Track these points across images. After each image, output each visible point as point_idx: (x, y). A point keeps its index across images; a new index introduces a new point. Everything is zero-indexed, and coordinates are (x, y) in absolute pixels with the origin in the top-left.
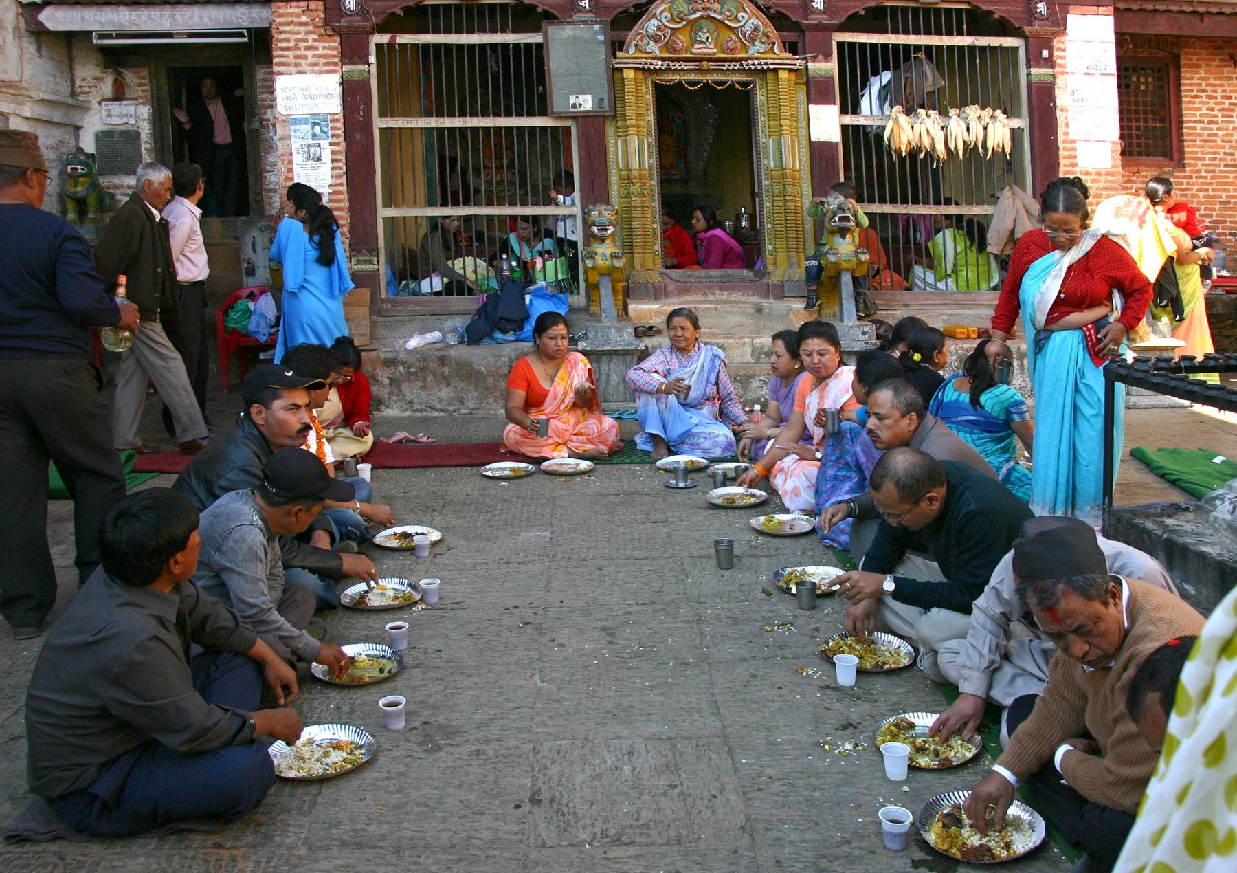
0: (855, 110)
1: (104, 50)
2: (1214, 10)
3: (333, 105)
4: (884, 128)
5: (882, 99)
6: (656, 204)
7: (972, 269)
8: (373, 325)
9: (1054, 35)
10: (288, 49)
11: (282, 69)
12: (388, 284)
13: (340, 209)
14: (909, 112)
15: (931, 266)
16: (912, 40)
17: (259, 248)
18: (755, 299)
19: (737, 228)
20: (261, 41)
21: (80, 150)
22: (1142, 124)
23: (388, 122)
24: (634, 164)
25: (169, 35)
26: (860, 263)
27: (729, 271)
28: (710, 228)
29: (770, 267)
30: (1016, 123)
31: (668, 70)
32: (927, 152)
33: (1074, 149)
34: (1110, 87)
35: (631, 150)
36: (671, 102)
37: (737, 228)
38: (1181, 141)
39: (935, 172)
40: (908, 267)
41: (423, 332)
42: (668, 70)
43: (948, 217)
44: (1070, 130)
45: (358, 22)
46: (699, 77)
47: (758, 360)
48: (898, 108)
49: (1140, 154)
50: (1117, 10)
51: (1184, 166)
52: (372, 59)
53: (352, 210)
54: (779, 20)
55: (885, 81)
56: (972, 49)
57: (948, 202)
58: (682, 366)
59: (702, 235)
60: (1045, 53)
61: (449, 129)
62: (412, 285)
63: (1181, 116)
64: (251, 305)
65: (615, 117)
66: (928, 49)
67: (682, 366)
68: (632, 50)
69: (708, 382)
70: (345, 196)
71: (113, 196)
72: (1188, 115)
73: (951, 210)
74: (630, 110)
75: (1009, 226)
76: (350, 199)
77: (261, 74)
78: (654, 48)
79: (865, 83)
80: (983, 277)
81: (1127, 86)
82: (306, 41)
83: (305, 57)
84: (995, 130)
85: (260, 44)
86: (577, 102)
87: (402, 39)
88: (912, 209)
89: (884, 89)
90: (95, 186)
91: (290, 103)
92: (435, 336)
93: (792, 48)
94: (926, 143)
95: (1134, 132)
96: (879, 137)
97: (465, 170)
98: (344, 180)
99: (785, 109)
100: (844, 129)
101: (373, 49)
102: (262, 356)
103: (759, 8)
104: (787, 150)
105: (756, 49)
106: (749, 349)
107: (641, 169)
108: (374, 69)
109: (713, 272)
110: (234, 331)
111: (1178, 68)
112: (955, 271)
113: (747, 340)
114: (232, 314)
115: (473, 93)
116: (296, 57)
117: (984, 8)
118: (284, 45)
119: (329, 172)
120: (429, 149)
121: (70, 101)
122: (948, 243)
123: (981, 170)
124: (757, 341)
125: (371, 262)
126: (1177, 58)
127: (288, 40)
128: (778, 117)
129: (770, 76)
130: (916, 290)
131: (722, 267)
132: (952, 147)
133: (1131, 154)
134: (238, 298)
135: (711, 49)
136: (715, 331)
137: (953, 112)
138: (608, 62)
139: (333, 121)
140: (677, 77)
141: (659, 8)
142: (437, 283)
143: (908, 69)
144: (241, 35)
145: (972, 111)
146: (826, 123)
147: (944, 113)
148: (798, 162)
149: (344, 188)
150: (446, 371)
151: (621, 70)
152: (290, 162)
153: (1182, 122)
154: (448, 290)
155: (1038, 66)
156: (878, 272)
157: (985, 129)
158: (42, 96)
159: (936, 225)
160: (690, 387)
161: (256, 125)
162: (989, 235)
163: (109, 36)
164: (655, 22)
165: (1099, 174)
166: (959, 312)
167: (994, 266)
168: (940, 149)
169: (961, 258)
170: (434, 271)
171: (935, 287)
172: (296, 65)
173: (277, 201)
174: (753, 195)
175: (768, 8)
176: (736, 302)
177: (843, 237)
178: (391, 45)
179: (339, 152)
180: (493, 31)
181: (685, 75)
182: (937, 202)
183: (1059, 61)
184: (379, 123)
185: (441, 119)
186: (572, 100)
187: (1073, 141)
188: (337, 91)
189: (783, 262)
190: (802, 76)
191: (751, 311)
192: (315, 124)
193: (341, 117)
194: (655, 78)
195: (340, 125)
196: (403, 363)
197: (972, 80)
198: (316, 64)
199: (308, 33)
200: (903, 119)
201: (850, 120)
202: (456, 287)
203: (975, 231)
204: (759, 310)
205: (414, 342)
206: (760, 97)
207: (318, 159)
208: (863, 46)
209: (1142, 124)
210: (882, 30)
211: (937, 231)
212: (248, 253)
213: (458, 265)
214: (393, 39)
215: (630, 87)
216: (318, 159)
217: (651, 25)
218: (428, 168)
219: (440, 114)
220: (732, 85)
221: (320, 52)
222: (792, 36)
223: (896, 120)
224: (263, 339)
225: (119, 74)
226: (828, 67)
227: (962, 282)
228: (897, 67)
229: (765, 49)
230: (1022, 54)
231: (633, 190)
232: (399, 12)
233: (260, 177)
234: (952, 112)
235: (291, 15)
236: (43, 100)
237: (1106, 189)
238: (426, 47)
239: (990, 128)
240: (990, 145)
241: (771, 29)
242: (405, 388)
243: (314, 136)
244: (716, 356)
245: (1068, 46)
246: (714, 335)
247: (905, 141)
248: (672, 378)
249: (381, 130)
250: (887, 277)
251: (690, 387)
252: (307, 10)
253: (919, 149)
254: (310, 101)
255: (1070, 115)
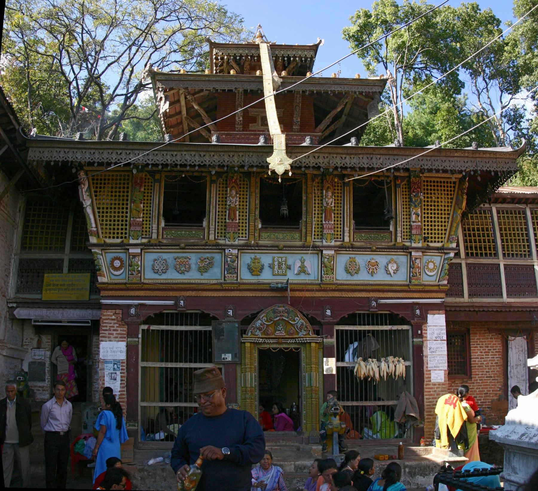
0: (343, 360)
1: (35, 326)
2: (481, 310)
3: (123, 356)
4: (354, 367)
5: (354, 354)
6: (257, 403)
7: (388, 428)
8: (135, 453)
9: (423, 323)
10: (106, 330)
11: (103, 339)
12: (142, 435)
13: (123, 402)
14: (364, 360)
15: (371, 428)
16: (367, 328)
17: (89, 418)
18: (297, 444)
19: (291, 412)
20: (96, 325)
21: (23, 370)
22: (456, 360)
23: (145, 364)
24: (248, 385)
25: (60, 322)
26: (342, 428)
27: (287, 432)
28: (280, 412)
29: (304, 430)
30: (408, 363)
31: (264, 343)
32: (372, 378)
33: (430, 374)
34: (444, 346)
35: (247, 378)
36: (265, 357)
37: (291, 412)
38: (470, 367)
39: (375, 386)
40: (362, 429)
41: (155, 457)
42: (264, 343)
43: (379, 406)
44: (429, 366)
45: (135, 319)
46: (278, 346)
47: (297, 471)
48: (360, 358)
49: (455, 374)
50: (446, 311)
51: (471, 378)
52: (140, 336)
53: (128, 403)
54: (312, 321)
55: (355, 346)
56: (391, 331)
57: (379, 399)
58: (264, 475)
59: (277, 416)
60: (419, 332)
61: (171, 368)
62: (152, 436)
63: (470, 356)
64: (85, 442)
65: (241, 364)
66: (373, 331)
67: (264, 475)
68: (250, 334)
69: (275, 482)
70: (125, 396)
71: (33, 390)
72: (473, 355)
73: (380, 403)
74: (247, 361)
75: (403, 409)
76: (127, 398)
77: (94, 340)
78: (259, 333)
79: (347, 347)
80: (392, 432)
81: (451, 344)
82: (113, 327)
83: (113, 334)
84: (399, 367)
85: (95, 326)
86: (225, 357)
87: (153, 327)
88: (365, 403)
89: (355, 350)
90: (27, 386)
91: (105, 354)
92: (160, 459)
93: (317, 333)
94: (371, 373)
95: (453, 364)
96: (352, 371)
97: (176, 384)
98: (125, 389)
99: (313, 360)
100: (338, 368)
101: (140, 331)
102: (88, 466)
103: (304, 315)
104: (313, 379)
105: (302, 333)
106: (293, 466)
107: (251, 387)
108: (140, 340)
109: (280, 433)
110: (78, 454)
111: (469, 334)
112: (381, 430)
113: (293, 463)
114: (77, 446)
115: (181, 350)
116: (109, 334)
117: (396, 313)
118: (105, 328)
119: (119, 385)
120: (161, 375)
121: (20, 348)
122: (379, 417)
123: (392, 382)
124: (297, 463)
125: (135, 426)
126: (468, 330)
127: (106, 326)
128: (310, 364)
129: (307, 345)
130: (364, 439)
131: (284, 430)
132: (382, 375)
133: (452, 373)
134: (79, 439)
135: (283, 334)
136: (279, 458)
137: (383, 359)
138: (239, 339)
139: (122, 363)
140: (268, 346)
141: (262, 315)
142: (162, 435)
143: (365, 341)
144: (88, 323)
145: (390, 359)
146: (330, 365)
147: (379, 360)
148: (317, 383)
149: (125, 393)
150: (165, 474)
151: (244, 343)
152: (104, 380)
153: (471, 358)
154: (167, 439)
155: (417, 338)
156: (349, 431)
157: (395, 366)
158: (11, 346)
159: (374, 410)
160: (267, 485)
161: (91, 363)
162: (395, 414)
163: (38, 321)
164: (260, 321)
165: (439, 385)
166: (382, 448)
167: (396, 427)
168: (377, 376)
169: (384, 423)
170: (161, 429)
171: (372, 437)
172: (109, 337)
173: (98, 397)
174: (299, 397)
175: (308, 315)
176: (289, 446)
177: (335, 417)
178: (148, 330)
179: (124, 377)
180: (191, 325)
181: (271, 345)
182: (375, 400)
183: (425, 335)
184: (141, 364)
185: (167, 363)
186: (223, 356)
187: (430, 371)
188: (124, 349)
189: (309, 425)
190: (321, 345)
191: (295, 449)
192: (115, 364)
193: (125, 361)
194: (259, 346)
195: (125, 364)
196: (147, 471)
197: (390, 346)
198: (116, 337)
199: (115, 323)
200: (362, 363)
201: (340, 364)
202: (169, 437)
203: (389, 411)
204: (298, 449)
205: (151, 462)
206: (303, 355)
207: (115, 379)
208: (347, 331)
209: (456, 360)
210: (354, 324)
211: (374, 412)
212: (85, 419)
213: (171, 427)
214: (149, 327)
215: (248, 350)
216: (115, 379)
217: (258, 323)
218: (161, 383)
219: (167, 361)
220: (292, 349)
221: (119, 332)
222: (317, 327)
223: (359, 364)
224: (89, 457)
225: (40, 337)
226: (332, 341)
227: (383, 435)
228: (360, 340)
229: (306, 335)
230: (410, 332)
231: (248, 396)
232: (153, 316)
233: (91, 385)
234: (383, 359)
235: (108, 315)
236: (11, 348)
237: (442, 391)
238: (162, 331)
239: (398, 366)
240: (397, 374)
241: (308, 324)
242: (147, 481)
243: (114, 369)
244: (279, 471)
245: (428, 328)
246: (279, 461)
247: (363, 373)
248: (259, 480)
249: (142, 368)
250: (353, 433)
251: (267, 485)
252: (115, 314)
253: (369, 376)
254: (113, 354)
255: (429, 359)
